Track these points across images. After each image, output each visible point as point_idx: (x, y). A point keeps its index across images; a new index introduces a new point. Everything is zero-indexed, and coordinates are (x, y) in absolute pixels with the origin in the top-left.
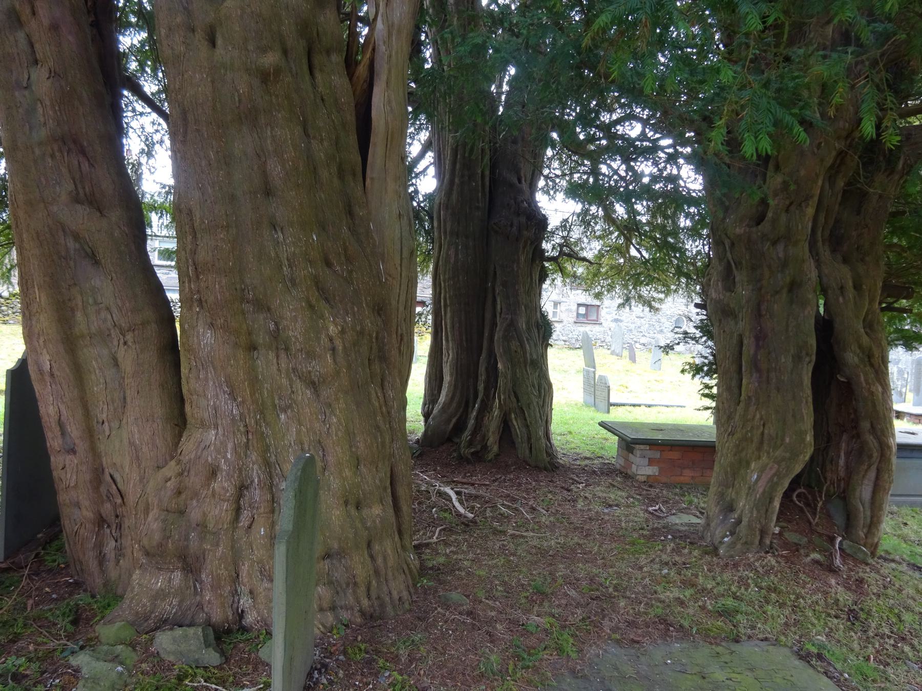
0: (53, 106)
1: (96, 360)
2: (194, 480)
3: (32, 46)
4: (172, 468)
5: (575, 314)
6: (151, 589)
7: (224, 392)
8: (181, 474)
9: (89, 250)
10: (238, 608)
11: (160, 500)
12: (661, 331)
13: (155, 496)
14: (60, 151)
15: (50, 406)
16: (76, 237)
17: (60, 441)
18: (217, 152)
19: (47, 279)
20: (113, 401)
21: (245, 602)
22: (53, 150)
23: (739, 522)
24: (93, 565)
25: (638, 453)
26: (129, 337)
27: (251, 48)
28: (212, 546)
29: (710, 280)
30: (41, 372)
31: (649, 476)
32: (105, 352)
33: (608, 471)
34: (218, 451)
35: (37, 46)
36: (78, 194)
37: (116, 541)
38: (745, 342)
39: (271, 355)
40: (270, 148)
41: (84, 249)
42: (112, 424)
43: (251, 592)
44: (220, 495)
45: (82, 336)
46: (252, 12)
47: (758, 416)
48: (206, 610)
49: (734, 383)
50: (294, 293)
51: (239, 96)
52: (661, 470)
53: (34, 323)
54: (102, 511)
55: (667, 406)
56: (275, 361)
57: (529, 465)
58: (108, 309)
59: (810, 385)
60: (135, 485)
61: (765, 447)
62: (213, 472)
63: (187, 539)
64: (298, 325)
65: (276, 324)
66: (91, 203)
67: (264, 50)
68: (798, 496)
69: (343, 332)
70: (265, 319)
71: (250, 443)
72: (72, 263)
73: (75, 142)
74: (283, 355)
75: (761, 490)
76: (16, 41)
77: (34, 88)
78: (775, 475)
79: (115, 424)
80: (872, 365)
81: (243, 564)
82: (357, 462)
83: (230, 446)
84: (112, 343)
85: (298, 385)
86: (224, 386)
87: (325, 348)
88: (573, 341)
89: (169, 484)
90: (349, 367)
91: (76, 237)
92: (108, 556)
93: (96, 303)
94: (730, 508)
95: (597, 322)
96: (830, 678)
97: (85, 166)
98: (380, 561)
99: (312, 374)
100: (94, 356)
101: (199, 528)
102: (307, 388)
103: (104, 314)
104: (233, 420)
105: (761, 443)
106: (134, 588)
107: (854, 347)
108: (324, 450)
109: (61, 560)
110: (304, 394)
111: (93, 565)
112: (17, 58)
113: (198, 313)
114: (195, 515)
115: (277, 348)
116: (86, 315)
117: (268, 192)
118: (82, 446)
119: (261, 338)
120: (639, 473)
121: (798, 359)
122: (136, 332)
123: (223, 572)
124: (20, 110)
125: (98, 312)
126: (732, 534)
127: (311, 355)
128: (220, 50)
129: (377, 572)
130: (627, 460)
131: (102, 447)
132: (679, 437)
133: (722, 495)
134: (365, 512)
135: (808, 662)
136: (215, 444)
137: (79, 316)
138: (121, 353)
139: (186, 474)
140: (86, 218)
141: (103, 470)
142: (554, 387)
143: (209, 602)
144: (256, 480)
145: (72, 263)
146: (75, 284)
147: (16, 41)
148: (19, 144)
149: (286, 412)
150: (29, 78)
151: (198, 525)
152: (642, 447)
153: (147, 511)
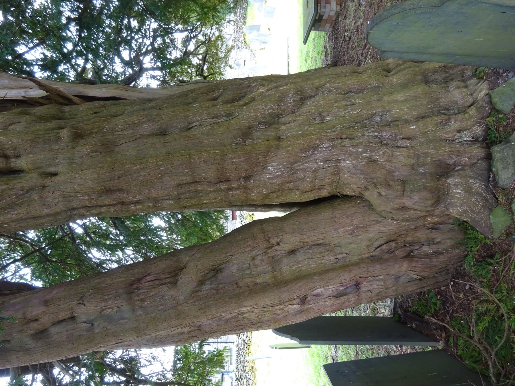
0: (105, 300)
1: (291, 267)
2: (380, 175)
3: (61, 321)
4: (371, 195)
6: (465, 196)
7: (313, 154)
8: (375, 185)
9: (211, 275)
10: (471, 141)
11: (397, 197)
13: (393, 202)
14: (138, 295)
16: (202, 283)
17: (351, 296)
18: (134, 164)
19: (233, 301)
20: (321, 252)
21: (466, 135)
22: (138, 300)
24: (443, 258)
25: (323, 10)
26: (273, 241)
27: (57, 147)
28: (428, 157)
30: (301, 312)
31: (337, 4)
32: (285, 260)
33: (334, 36)
34: (357, 158)
35: (61, 317)
36: (170, 283)
37: (423, 245)
39: (283, 127)
40: (131, 131)
41: (211, 278)
42: (338, 252)
43: (459, 131)
44: (389, 156)
45: (275, 277)
46: (30, 146)
48: (475, 161)
51: (92, 152)
53: (265, 319)
54: (402, 256)
56: (287, 125)
58: (253, 259)
60: (384, 226)
62: (372, 161)
63: (424, 174)
65: (260, 123)
66: (176, 275)
67: (58, 139)
69: (263, 85)
70: (257, 131)
71: (349, 136)
72: (221, 286)
73: (131, 285)
74: (283, 120)
76: (58, 333)
77: (92, 318)
79: (338, 250)
81: (439, 136)
83: (352, 150)
84: (278, 255)
85: (304, 109)
86: (307, 154)
87: (276, 91)
89: (383, 193)
91: (202, 283)
92: (435, 250)
93: (249, 268)
99: (295, 99)
101: (415, 168)
102: (306, 104)
103: (257, 262)
104: (333, 146)
106: (464, 210)
108: (350, 92)
109: (434, 301)
111: (443, 258)
112: (71, 332)
113: (255, 181)
114: (403, 173)
115: (278, 124)
116: (259, 274)
117: (163, 133)
118: (357, 272)
120: (335, 9)
122: (270, 236)
123: (447, 148)
124: (109, 327)
125: (256, 266)
127: (282, 99)
128: (59, 169)
130: (327, 21)
131: (355, 258)
134: (391, 66)
136: (352, 160)
137: (259, 280)
138: (285, 247)
139: (375, 181)
140: (187, 276)
141: (372, 256)
143: (469, 158)
144: (376, 134)
145: (221, 286)
146: (236, 283)
147: (58, 333)
148: (134, 326)
149: (325, 117)
150: (85, 322)
151: (413, 169)
152: (319, 8)
153: (404, 208)
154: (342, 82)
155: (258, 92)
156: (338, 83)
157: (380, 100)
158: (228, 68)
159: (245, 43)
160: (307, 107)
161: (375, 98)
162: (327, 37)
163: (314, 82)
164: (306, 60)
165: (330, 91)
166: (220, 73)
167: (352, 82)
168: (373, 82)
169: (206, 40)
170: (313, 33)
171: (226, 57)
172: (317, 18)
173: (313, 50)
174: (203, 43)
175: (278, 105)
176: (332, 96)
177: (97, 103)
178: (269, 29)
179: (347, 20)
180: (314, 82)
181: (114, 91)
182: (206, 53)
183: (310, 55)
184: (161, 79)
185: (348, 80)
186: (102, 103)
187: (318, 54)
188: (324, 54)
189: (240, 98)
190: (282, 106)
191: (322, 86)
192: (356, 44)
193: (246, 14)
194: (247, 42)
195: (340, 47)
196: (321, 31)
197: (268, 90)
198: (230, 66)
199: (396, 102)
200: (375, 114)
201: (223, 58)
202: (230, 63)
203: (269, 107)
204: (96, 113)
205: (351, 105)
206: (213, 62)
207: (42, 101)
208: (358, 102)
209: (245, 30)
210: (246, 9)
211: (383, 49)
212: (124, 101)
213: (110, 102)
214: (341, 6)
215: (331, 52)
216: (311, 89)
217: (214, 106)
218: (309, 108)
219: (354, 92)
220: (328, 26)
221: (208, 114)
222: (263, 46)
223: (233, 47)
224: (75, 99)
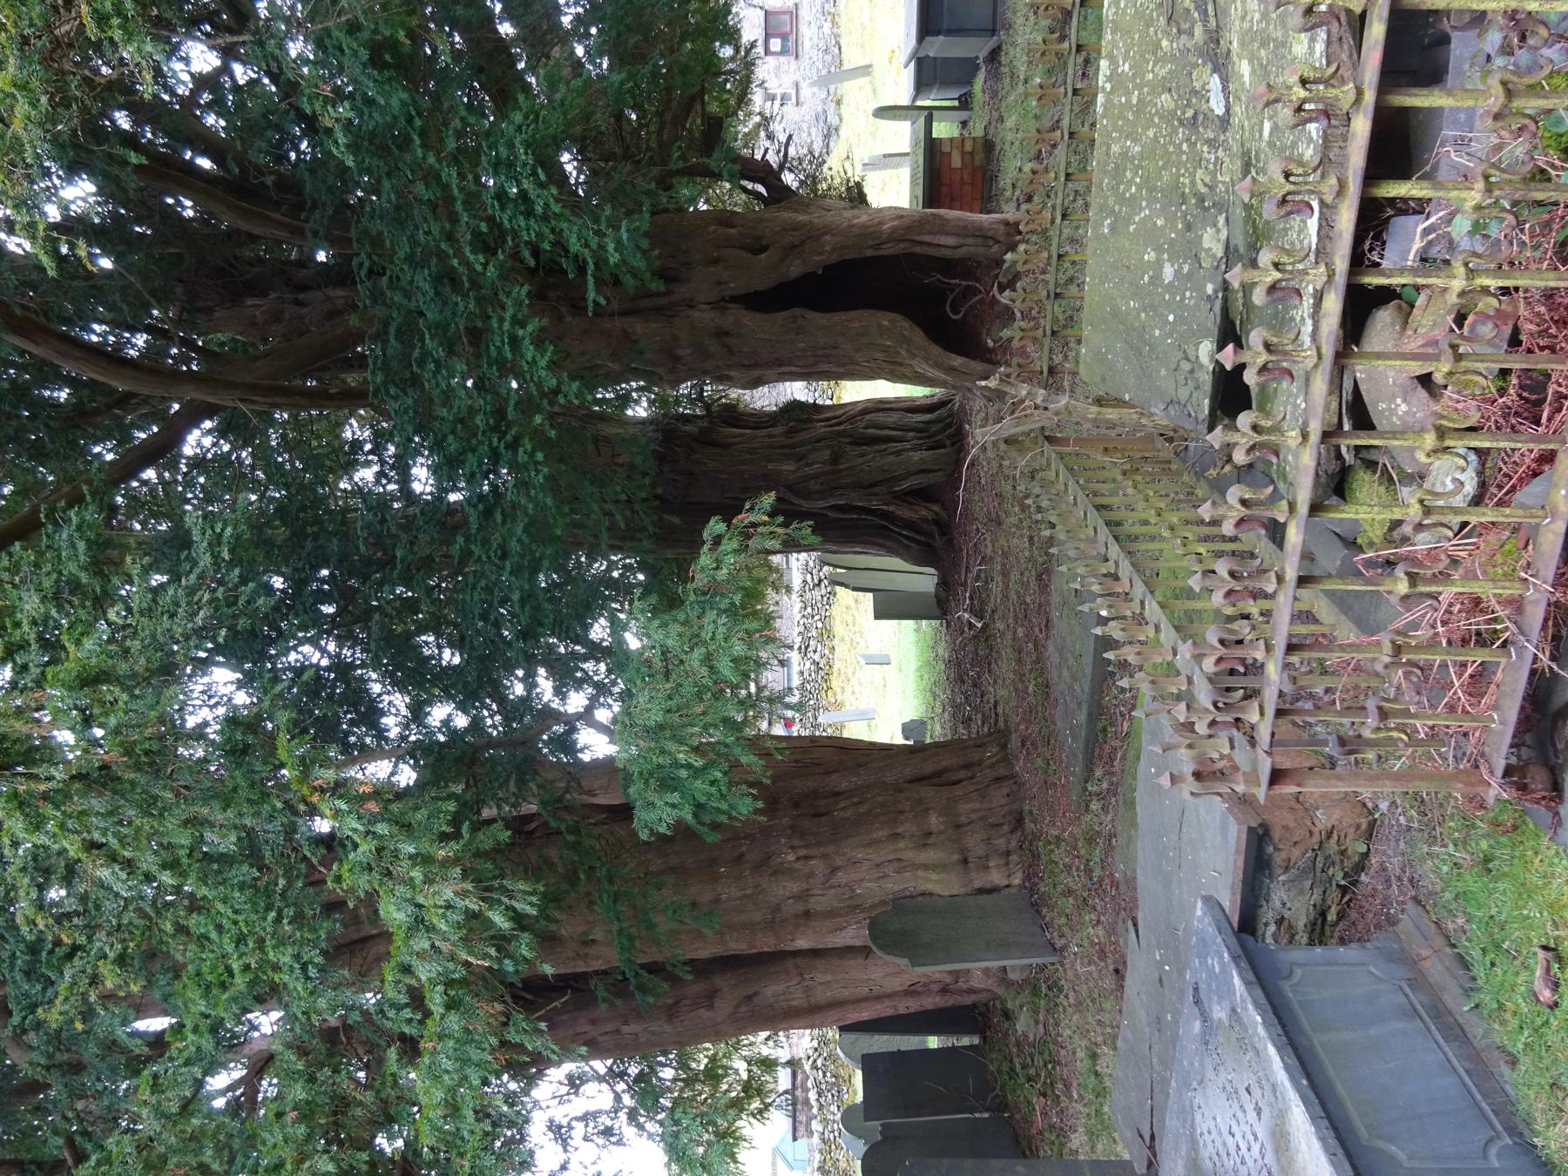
5: (782, 59)
15: (865, 1015)
16: (738, 1006)
39: (813, 900)
59: (828, 315)
68: (957, 313)
69: (792, 848)
80: (803, 243)
82: (896, 837)
88: (829, 57)
90: (819, 844)
95: (794, 14)
97: (686, 1002)
98: (973, 816)
100: (822, 995)
110: (841, 878)
119: (800, 908)
127: (811, 875)
129: (983, 818)
131: (889, 991)
137: (794, 1003)
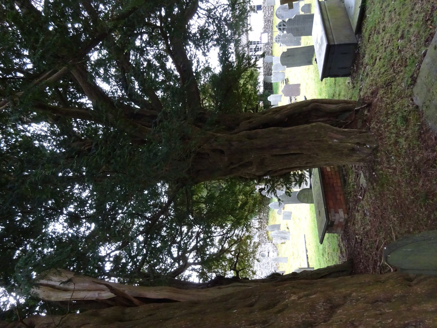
12: (268, 263)
23: (358, 144)
25: (333, 218)
29: (248, 173)
31: (344, 213)
33: (346, 236)
38: (275, 153)
47: (307, 144)
49: (294, 157)
50: (272, 321)
52: (340, 208)
55: (306, 243)
57: (352, 271)
61: (321, 139)
64: (294, 315)
69: (294, 293)
75: (341, 136)
78: (333, 132)
85: (335, 318)
94: (353, 150)
96: (420, 67)
105: (319, 141)
107: (274, 116)
108: (378, 301)
121: (280, 133)
126: (365, 145)
127: (313, 308)
130: (337, 226)
132: (322, 201)
133: (348, 155)
135: (416, 78)
142: (313, 98)
152: (330, 216)
154: (368, 291)
155: (290, 299)
156: (364, 292)
157: (410, 309)
158: (256, 261)
159: (268, 238)
160: (338, 316)
161: (403, 307)
162: (340, 238)
163: (340, 290)
164: (323, 255)
165: (358, 300)
166: (249, 265)
167: (376, 291)
168: (399, 292)
169: (238, 239)
170: (327, 235)
171: (254, 252)
172: (329, 224)
173: (328, 247)
174: (236, 242)
175: (310, 313)
176: (360, 305)
177: (152, 306)
178: (288, 228)
179: (356, 226)
180: (340, 290)
181: (166, 293)
182: (238, 248)
183: (326, 250)
184: (200, 271)
185: (373, 289)
186: (157, 305)
187: (334, 250)
188: (339, 251)
189: (274, 305)
190: (314, 314)
191: (350, 295)
192: (368, 246)
193: (268, 217)
194: (270, 237)
195: (353, 246)
196: (334, 233)
197: (300, 298)
198: (257, 260)
199: (426, 312)
200: (408, 324)
201: (252, 253)
202: (257, 256)
203: (302, 315)
204: (151, 315)
205: (381, 314)
206: (243, 256)
207: (110, 302)
208: (387, 311)
209: (267, 228)
210: (268, 213)
211: (403, 268)
212: (174, 303)
213: (162, 304)
214: (348, 214)
215: (346, 250)
216: (339, 298)
217: (251, 312)
218: (340, 317)
219: (381, 301)
220: (339, 229)
221: (245, 321)
222: (283, 241)
223: (259, 244)
224: (135, 301)
